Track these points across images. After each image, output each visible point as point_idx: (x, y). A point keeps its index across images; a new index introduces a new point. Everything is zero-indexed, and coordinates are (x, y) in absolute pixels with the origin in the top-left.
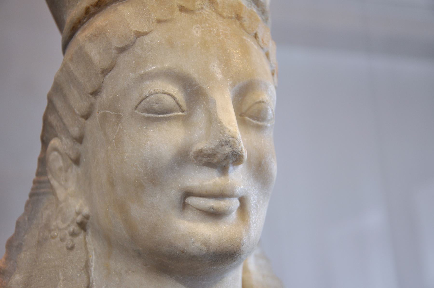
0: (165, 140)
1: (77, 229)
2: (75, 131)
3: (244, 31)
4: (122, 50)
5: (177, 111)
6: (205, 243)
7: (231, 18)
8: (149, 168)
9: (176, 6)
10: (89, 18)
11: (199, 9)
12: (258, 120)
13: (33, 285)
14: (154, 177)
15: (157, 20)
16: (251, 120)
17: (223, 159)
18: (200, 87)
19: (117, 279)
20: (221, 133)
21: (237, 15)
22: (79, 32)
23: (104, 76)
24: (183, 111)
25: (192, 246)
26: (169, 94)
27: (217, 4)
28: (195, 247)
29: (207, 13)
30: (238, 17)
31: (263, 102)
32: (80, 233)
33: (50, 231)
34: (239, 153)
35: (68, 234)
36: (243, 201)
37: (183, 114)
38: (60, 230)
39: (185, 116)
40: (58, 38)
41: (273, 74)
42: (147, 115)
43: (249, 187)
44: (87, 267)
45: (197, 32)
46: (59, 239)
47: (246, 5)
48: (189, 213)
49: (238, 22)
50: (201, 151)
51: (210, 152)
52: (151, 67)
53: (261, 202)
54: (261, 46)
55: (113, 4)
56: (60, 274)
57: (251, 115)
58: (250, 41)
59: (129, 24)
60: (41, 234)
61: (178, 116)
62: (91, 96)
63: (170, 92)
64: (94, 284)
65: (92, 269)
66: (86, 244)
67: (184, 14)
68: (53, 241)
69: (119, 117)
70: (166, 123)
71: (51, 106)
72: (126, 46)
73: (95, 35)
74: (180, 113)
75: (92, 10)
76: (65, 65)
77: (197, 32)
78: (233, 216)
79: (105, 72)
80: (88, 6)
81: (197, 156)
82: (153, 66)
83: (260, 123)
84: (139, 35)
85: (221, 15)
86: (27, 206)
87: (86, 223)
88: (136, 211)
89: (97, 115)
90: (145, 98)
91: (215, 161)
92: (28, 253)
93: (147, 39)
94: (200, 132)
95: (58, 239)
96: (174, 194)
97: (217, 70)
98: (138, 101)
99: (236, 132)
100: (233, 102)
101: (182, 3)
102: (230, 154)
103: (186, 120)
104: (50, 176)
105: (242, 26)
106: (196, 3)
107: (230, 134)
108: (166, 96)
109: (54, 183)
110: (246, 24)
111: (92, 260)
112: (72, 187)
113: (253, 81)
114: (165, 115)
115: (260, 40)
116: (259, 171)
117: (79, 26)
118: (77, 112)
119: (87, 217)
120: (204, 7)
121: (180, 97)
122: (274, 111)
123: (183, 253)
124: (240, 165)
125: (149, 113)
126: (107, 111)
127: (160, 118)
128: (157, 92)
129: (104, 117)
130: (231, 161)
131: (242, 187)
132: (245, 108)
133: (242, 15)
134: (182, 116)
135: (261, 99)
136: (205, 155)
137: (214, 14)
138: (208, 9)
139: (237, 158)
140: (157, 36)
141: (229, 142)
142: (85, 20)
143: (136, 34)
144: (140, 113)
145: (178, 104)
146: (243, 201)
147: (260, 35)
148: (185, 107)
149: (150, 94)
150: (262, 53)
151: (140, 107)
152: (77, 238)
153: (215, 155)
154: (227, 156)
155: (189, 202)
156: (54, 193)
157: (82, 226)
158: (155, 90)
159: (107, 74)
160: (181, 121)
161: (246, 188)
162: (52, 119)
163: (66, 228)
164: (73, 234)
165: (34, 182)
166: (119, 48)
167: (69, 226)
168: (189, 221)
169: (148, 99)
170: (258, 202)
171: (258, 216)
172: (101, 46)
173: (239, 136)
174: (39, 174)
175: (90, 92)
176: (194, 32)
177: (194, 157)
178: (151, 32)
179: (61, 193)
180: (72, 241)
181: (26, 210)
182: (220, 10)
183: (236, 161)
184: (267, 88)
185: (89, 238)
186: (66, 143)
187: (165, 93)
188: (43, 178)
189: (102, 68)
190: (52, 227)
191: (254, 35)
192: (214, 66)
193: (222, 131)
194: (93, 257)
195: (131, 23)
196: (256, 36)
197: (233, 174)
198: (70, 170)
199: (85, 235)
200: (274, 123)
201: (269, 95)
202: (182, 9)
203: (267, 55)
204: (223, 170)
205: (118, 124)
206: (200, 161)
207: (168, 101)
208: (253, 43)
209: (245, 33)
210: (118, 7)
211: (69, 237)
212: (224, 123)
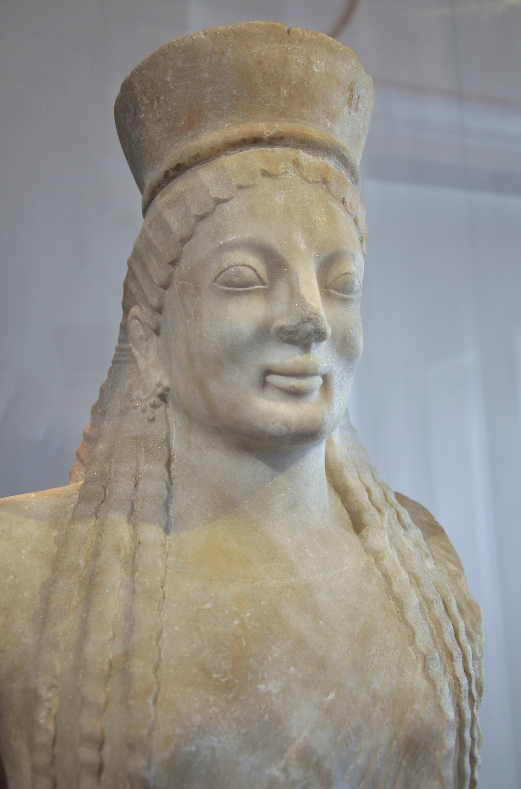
0: (244, 315)
1: (157, 400)
2: (154, 301)
3: (330, 196)
4: (201, 218)
5: (258, 285)
6: (285, 423)
7: (317, 182)
8: (228, 344)
9: (258, 170)
10: (169, 182)
11: (282, 174)
12: (344, 293)
13: (116, 456)
14: (233, 353)
15: (238, 185)
16: (337, 293)
17: (305, 336)
18: (282, 259)
19: (197, 454)
20: (303, 309)
21: (324, 179)
22: (158, 197)
23: (183, 245)
24: (264, 284)
25: (272, 426)
26: (249, 267)
27: (303, 167)
28: (275, 426)
29: (291, 177)
30: (325, 182)
31: (350, 273)
32: (161, 405)
33: (132, 401)
34: (322, 330)
35: (149, 405)
36: (326, 378)
37: (264, 287)
38: (141, 401)
39: (266, 289)
40: (137, 199)
41: (361, 241)
42: (226, 288)
43: (333, 364)
45: (280, 199)
46: (140, 410)
47: (334, 167)
48: (269, 392)
49: (324, 187)
50: (282, 328)
51: (291, 329)
52: (230, 238)
53: (346, 378)
54: (348, 212)
55: (192, 167)
56: (142, 446)
57: (335, 287)
58: (337, 208)
59: (209, 190)
60: (123, 403)
61: (258, 289)
63: (251, 263)
64: (175, 456)
65: (173, 441)
66: (167, 416)
67: (266, 179)
69: (197, 289)
70: (246, 297)
71: (131, 275)
72: (205, 213)
73: (174, 202)
75: (172, 174)
76: (143, 232)
77: (280, 199)
78: (316, 395)
79: (184, 241)
81: (279, 333)
82: (233, 236)
83: (345, 296)
84: (219, 202)
85: (306, 179)
86: (109, 373)
87: (167, 395)
88: (215, 388)
89: (176, 285)
90: (224, 271)
91: (297, 338)
92: (111, 423)
93: (227, 207)
94: (282, 307)
95: (139, 410)
96: (253, 372)
97: (301, 241)
98: (217, 274)
99: (319, 309)
100: (317, 274)
101: (264, 167)
102: (313, 332)
103: (267, 293)
104: (131, 345)
105: (329, 190)
106: (280, 167)
107: (313, 310)
108: (247, 269)
109: (136, 352)
110: (333, 188)
111: (173, 432)
112: (153, 356)
113: (339, 251)
114: (245, 289)
115: (348, 205)
116: (345, 347)
117: (158, 190)
118: (156, 282)
119: (167, 390)
120: (288, 171)
121: (261, 269)
122: (361, 282)
123: (263, 432)
124: (324, 342)
125: (228, 286)
127: (240, 292)
128: (237, 264)
129: (183, 288)
130: (313, 339)
131: (325, 364)
132: (330, 280)
133: (329, 179)
134: (263, 289)
135: (347, 271)
136: (286, 331)
137: (299, 178)
138: (292, 174)
139: (320, 335)
140: (238, 203)
141: (311, 319)
143: (215, 201)
144: (218, 286)
145: (259, 277)
146: (326, 378)
147: (348, 200)
148: (266, 280)
149: (230, 267)
150: (350, 220)
151: (219, 280)
152: (158, 410)
153: (297, 332)
154: (309, 334)
155: (270, 381)
156: (135, 362)
157: (163, 397)
158: (234, 262)
159: (185, 243)
160: (261, 295)
161: (330, 365)
162: (132, 286)
163: (146, 400)
164: (154, 406)
165: (117, 349)
166: (198, 216)
168: (269, 400)
169: (227, 272)
170: (343, 378)
171: (343, 394)
172: (180, 214)
173: (322, 312)
174: (120, 341)
175: (168, 261)
176: (277, 198)
177: (275, 334)
178: (231, 198)
179: (142, 363)
181: (109, 377)
182: (305, 174)
183: (318, 338)
184: (354, 257)
185: (170, 411)
187: (245, 266)
188: (124, 346)
189: (180, 237)
190: (134, 397)
191: (341, 200)
192: (297, 236)
193: (304, 307)
194: (174, 430)
195: (210, 189)
196: (343, 201)
197: (316, 351)
198: (150, 340)
199: (166, 407)
200: (361, 295)
201: (356, 267)
202: (265, 174)
203: (356, 221)
204: (306, 347)
205: (196, 296)
206: (281, 338)
207: (248, 273)
208: (340, 209)
209: (332, 198)
210: (198, 172)
211: (150, 409)
212: (307, 299)
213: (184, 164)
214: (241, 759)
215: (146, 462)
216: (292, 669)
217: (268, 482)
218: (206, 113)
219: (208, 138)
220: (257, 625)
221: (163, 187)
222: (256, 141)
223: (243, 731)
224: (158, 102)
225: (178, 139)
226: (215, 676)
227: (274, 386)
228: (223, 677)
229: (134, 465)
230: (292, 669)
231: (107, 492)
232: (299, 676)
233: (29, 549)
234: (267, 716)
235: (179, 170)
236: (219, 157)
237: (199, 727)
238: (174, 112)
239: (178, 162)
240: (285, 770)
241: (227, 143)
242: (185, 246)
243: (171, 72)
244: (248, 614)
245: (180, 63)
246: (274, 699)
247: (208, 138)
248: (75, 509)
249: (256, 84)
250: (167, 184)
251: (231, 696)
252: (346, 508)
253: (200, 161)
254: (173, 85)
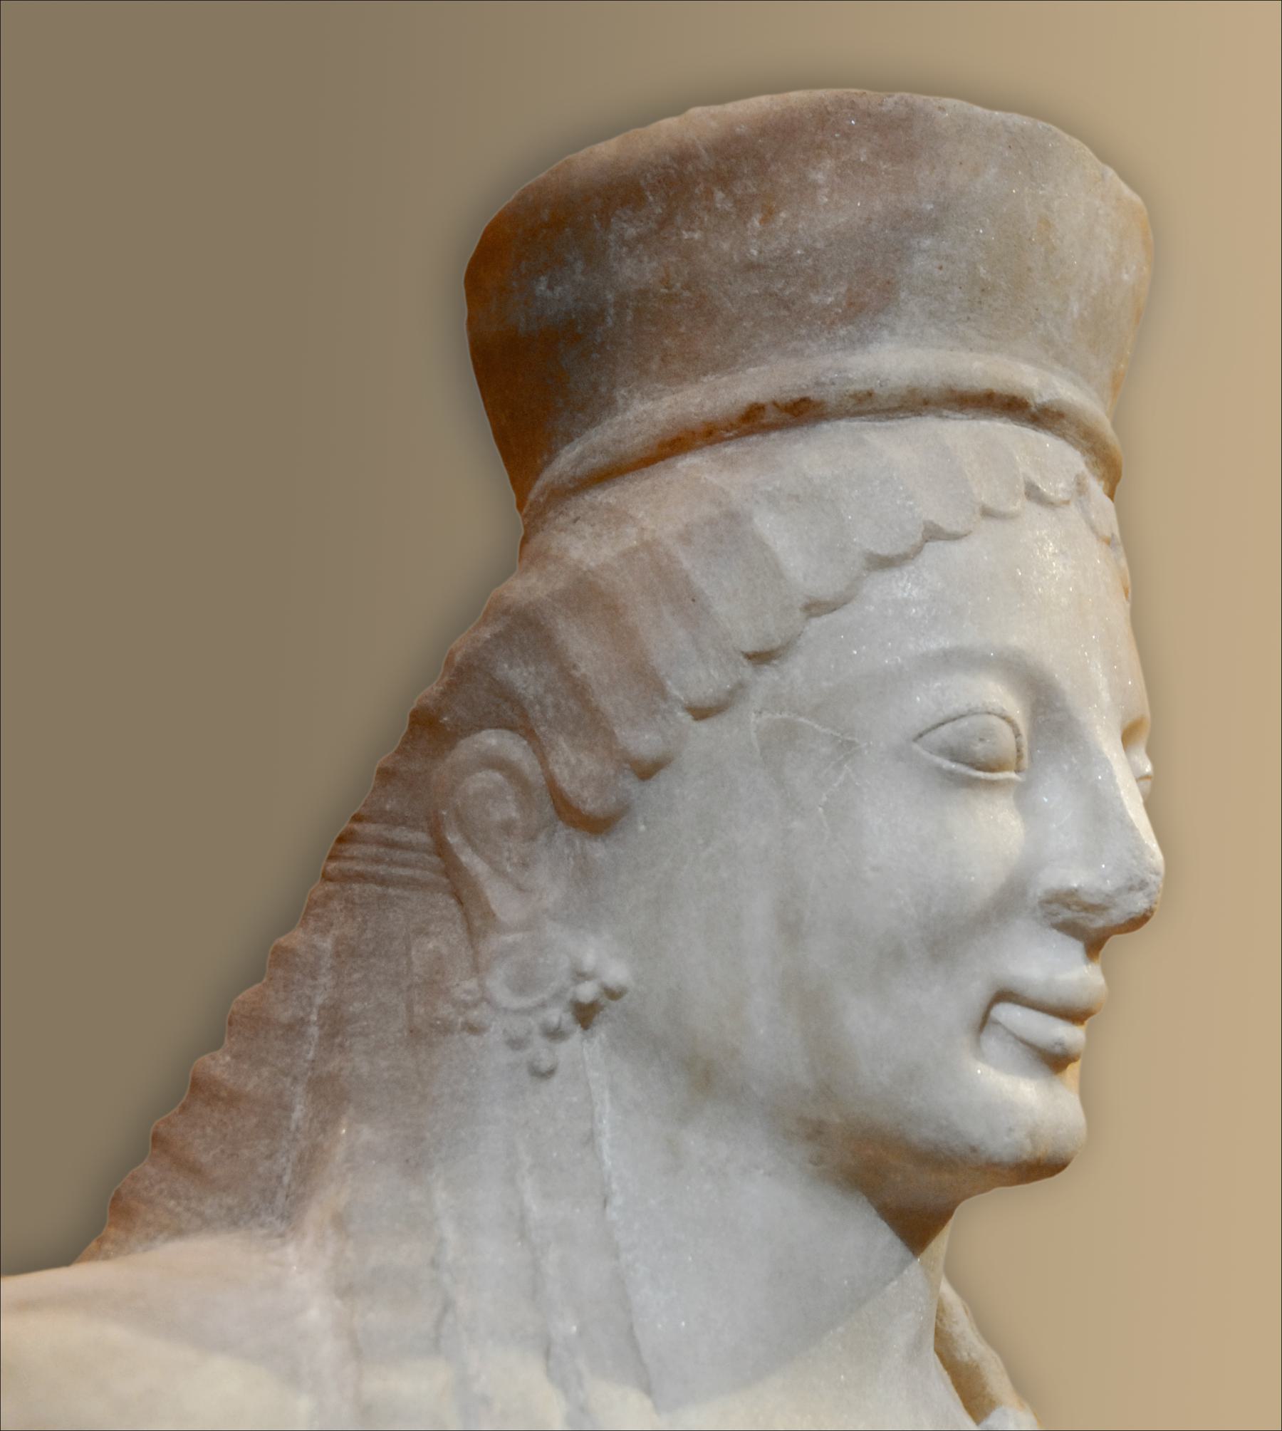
1: (568, 1018)
10: (749, 433)
20: (1134, 857)
35: (536, 1029)
42: (947, 765)
51: (1096, 900)
61: (1009, 781)
62: (745, 662)
64: (614, 1186)
74: (1013, 775)
75: (771, 416)
80: (762, 401)
84: (934, 534)
89: (752, 719)
90: (954, 719)
96: (977, 992)
98: (931, 722)
119: (613, 994)
126: (802, 720)
127: (977, 780)
142: (728, 435)
144: (925, 753)
149: (972, 712)
151: (933, 737)
159: (818, 615)
164: (555, 1034)
166: (878, 556)
167: (543, 1005)
169: (964, 723)
186: (573, 761)
198: (542, 838)
213: (821, 404)
217: (892, 1280)
218: (903, 295)
219: (892, 359)
221: (722, 440)
222: (1010, 406)
224: (764, 221)
225: (803, 332)
227: (1005, 1028)
236: (920, 415)
238: (810, 261)
239: (802, 395)
241: (952, 391)
247: (892, 359)
249: (1029, 269)
250: (737, 436)
253: (869, 412)
254: (829, 197)
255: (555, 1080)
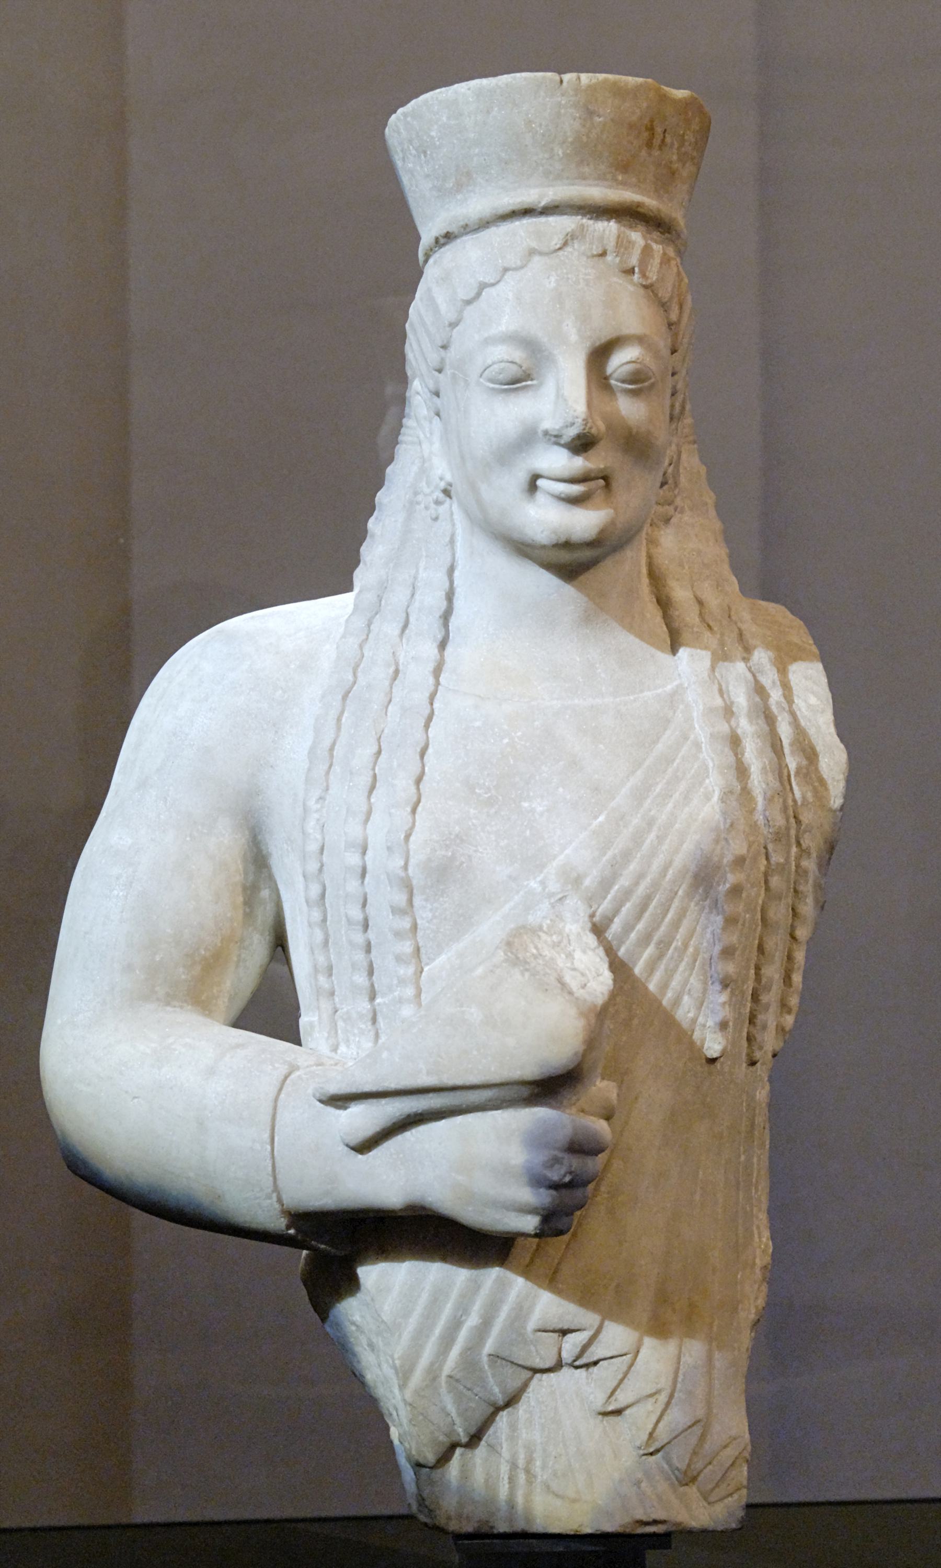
38: (426, 495)
42: (492, 385)
44: (452, 541)
66: (452, 514)
68: (418, 507)
73: (442, 279)
75: (442, 241)
79: (453, 325)
95: (422, 506)
96: (521, 476)
149: (494, 363)
157: (447, 492)
164: (438, 503)
167: (432, 492)
180: (436, 510)
194: (459, 531)
211: (433, 506)
214: (498, 869)
215: (425, 569)
216: (561, 790)
220: (528, 744)
223: (502, 844)
224: (425, 156)
226: (477, 791)
228: (486, 793)
229: (413, 572)
230: (561, 790)
231: (383, 602)
232: (568, 797)
233: (298, 663)
234: (528, 833)
235: (449, 238)
237: (457, 836)
240: (543, 883)
242: (455, 330)
243: (436, 127)
244: (519, 734)
245: (444, 119)
246: (537, 817)
248: (347, 621)
251: (493, 811)
252: (666, 624)
255: (439, 521)
